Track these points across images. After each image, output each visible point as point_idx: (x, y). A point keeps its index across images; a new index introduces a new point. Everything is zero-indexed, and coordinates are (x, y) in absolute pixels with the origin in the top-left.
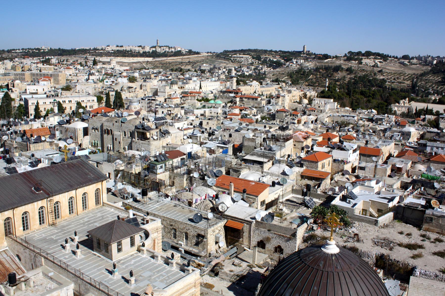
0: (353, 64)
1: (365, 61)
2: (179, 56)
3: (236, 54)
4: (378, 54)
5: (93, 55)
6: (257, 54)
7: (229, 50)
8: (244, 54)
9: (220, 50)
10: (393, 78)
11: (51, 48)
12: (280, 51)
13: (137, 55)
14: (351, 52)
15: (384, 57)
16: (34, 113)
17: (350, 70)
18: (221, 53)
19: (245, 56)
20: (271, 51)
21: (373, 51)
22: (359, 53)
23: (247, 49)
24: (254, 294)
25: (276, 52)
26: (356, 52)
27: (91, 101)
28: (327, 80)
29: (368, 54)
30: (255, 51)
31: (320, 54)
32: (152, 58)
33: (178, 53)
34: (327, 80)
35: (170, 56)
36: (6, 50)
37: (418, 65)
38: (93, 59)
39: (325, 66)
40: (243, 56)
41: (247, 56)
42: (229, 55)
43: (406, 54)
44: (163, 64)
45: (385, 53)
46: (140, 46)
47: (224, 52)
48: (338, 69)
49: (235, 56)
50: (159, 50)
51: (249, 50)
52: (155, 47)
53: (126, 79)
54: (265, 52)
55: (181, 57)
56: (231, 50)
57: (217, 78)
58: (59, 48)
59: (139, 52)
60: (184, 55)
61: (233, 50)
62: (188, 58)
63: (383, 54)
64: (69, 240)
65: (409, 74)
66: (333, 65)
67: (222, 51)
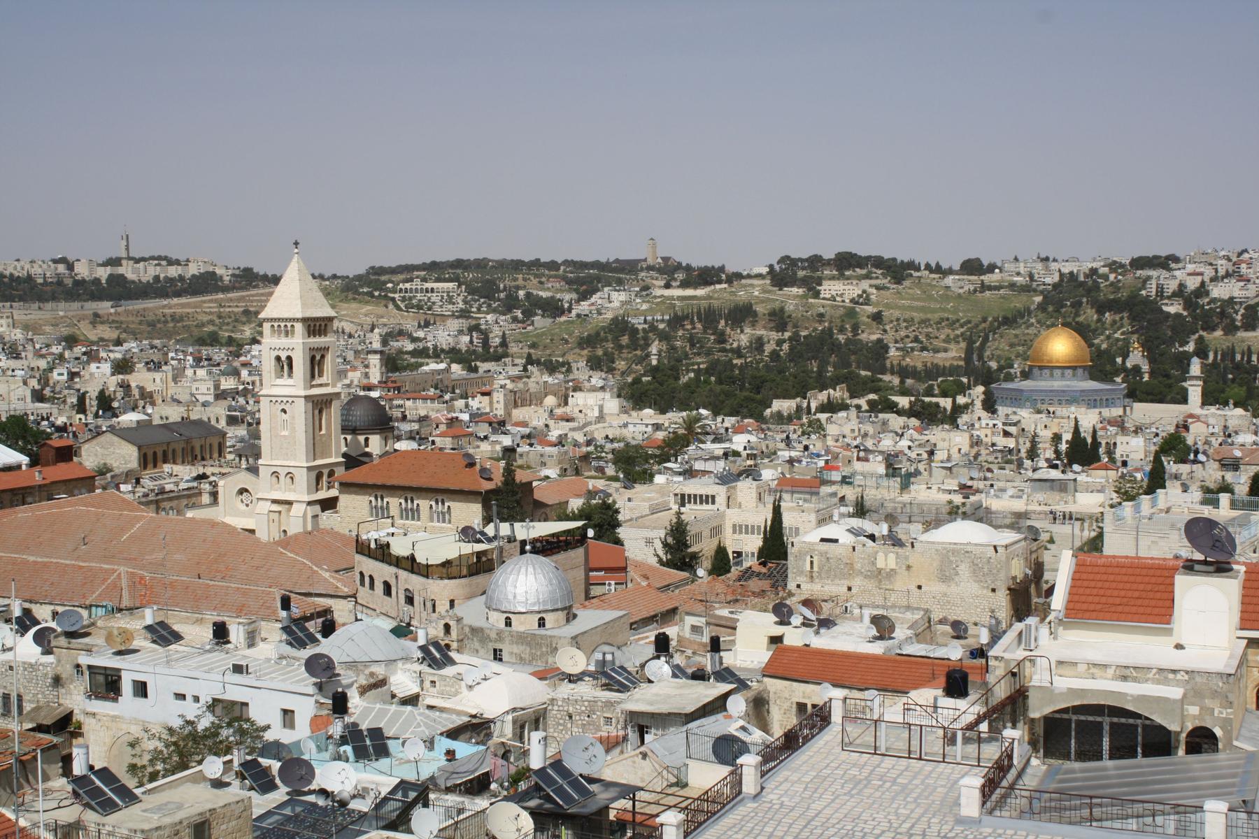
1: (830, 288)
2: (211, 292)
3: (411, 280)
4: (879, 262)
7: (386, 265)
8: (438, 280)
10: (912, 335)
12: (566, 262)
13: (53, 293)
14: (788, 257)
15: (897, 271)
16: (648, 411)
17: (779, 319)
20: (536, 263)
21: (863, 252)
22: (815, 262)
23: (452, 258)
24: (1253, 753)
25: (553, 265)
26: (805, 256)
29: (846, 263)
30: (480, 264)
32: (109, 304)
33: (206, 283)
35: (178, 294)
36: (829, 254)
37: (1002, 292)
40: (435, 285)
41: (451, 285)
42: (385, 283)
43: (973, 257)
44: (152, 324)
45: (903, 256)
46: (63, 260)
47: (368, 273)
48: (742, 314)
49: (408, 285)
50: (128, 271)
51: (459, 264)
52: (115, 262)
53: (378, 356)
55: (221, 296)
56: (394, 265)
59: (60, 283)
60: (225, 289)
61: (403, 263)
62: (241, 299)
63: (894, 260)
65: (969, 322)
67: (361, 270)
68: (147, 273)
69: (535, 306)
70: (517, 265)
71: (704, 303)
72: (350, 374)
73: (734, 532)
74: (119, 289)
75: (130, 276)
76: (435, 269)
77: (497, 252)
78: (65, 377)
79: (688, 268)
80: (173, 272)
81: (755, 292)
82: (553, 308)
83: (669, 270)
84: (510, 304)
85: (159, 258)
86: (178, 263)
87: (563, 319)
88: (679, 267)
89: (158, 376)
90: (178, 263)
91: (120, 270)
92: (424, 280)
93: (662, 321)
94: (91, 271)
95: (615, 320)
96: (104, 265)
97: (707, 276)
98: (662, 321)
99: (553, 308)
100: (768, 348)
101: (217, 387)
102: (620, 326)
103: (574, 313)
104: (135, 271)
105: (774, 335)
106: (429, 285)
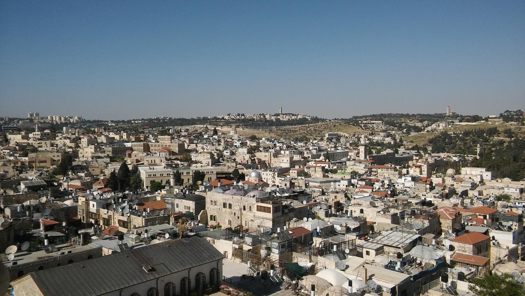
0: (512, 125)
5: (214, 125)
6: (391, 121)
9: (349, 116)
11: (316, 117)
17: (509, 133)
18: (350, 119)
19: (376, 122)
27: (152, 176)
28: (478, 146)
30: (390, 115)
31: (468, 116)
33: (303, 121)
34: (478, 146)
38: (213, 128)
39: (475, 129)
40: (375, 122)
41: (380, 122)
46: (263, 114)
48: (493, 131)
49: (366, 122)
50: (280, 118)
52: (279, 115)
54: (407, 116)
57: (333, 146)
58: (316, 117)
60: (309, 123)
64: (247, 208)
66: (487, 128)
68: (286, 118)
69: (409, 129)
70: (402, 116)
71: (477, 128)
72: (350, 154)
73: (211, 219)
74: (279, 123)
75: (281, 119)
76: (375, 117)
77: (394, 111)
78: (229, 154)
79: (461, 116)
80: (293, 117)
81: (498, 123)
82: (418, 129)
83: (455, 116)
84: (400, 128)
85: (290, 114)
86: (295, 115)
87: (422, 132)
88: (458, 116)
89: (267, 154)
90: (295, 115)
91: (279, 117)
92: (371, 120)
93: (461, 134)
94: (270, 117)
95: (442, 133)
96: (274, 116)
97: (476, 118)
98: (461, 134)
99: (418, 129)
100: (505, 145)
101: (291, 158)
102: (445, 134)
103: (426, 130)
104: (283, 118)
105: (508, 139)
106: (373, 122)
